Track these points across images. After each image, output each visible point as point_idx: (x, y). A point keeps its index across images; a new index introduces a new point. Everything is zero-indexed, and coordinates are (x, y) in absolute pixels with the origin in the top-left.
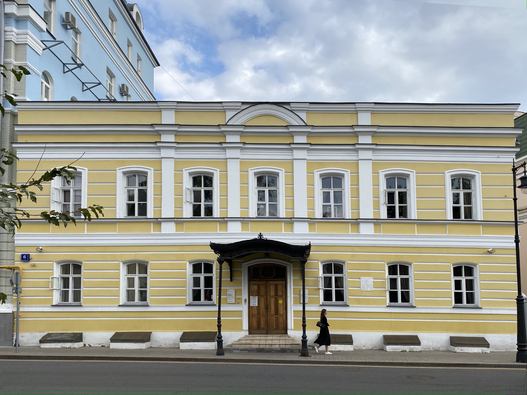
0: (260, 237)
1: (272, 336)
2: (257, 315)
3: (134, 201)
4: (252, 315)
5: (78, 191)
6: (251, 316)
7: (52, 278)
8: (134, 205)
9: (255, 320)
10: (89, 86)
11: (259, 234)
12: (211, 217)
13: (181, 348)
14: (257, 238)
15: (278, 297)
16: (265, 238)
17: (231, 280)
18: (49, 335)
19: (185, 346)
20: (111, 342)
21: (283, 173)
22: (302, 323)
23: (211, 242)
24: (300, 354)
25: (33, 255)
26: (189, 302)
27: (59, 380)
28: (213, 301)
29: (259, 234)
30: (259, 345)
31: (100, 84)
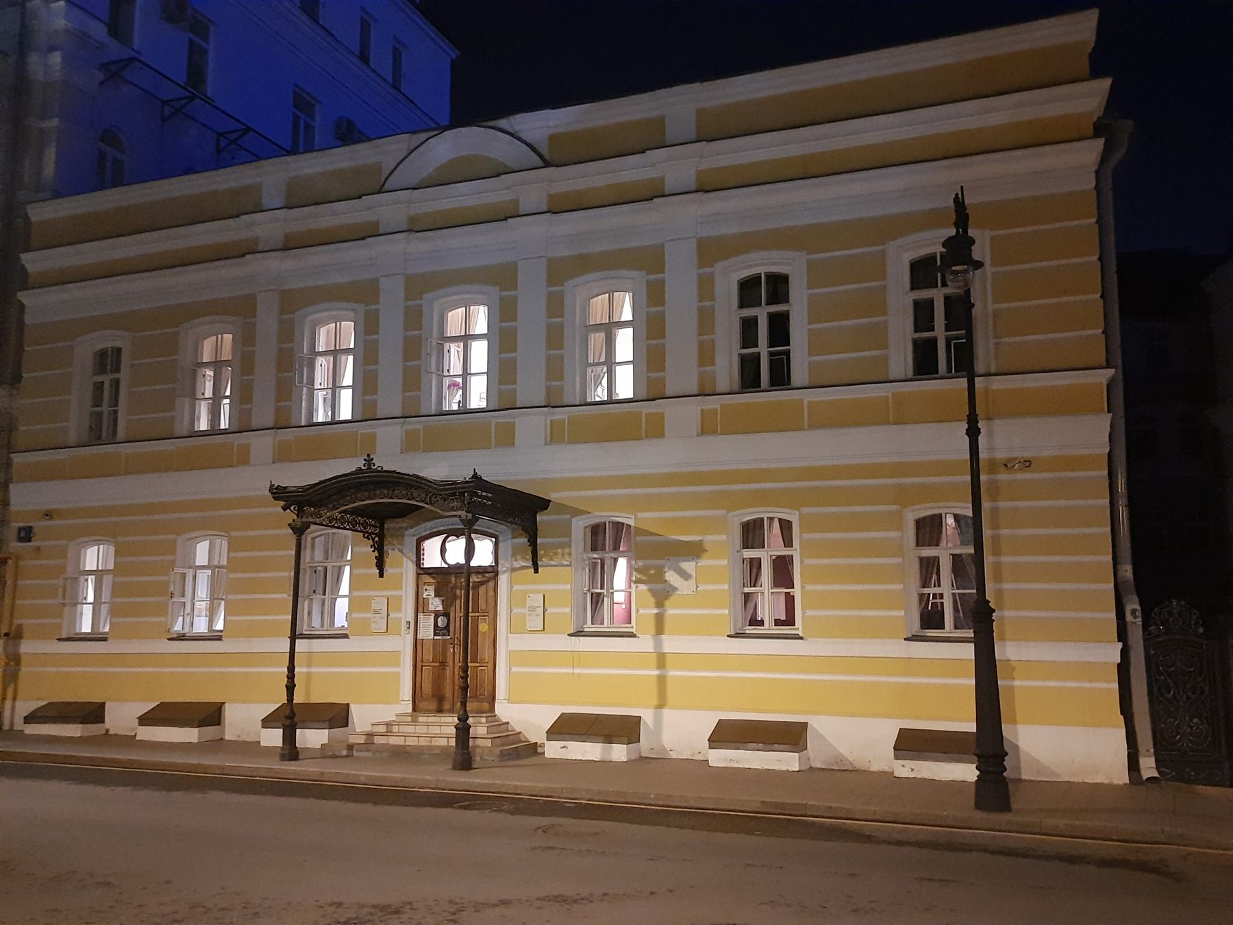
0: (369, 465)
1: (428, 716)
2: (433, 662)
3: (933, 330)
4: (422, 661)
5: (116, 384)
6: (419, 664)
7: (66, 579)
8: (933, 342)
9: (427, 674)
10: (233, 136)
11: (366, 458)
12: (789, 387)
13: (262, 744)
14: (363, 468)
15: (480, 614)
16: (379, 467)
17: (381, 575)
18: (163, 706)
19: (721, 758)
20: (141, 724)
21: (764, 265)
22: (286, 679)
23: (273, 483)
24: (278, 758)
25: (39, 525)
26: (735, 630)
27: (781, 867)
28: (796, 626)
29: (366, 458)
30: (404, 738)
31: (249, 129)
